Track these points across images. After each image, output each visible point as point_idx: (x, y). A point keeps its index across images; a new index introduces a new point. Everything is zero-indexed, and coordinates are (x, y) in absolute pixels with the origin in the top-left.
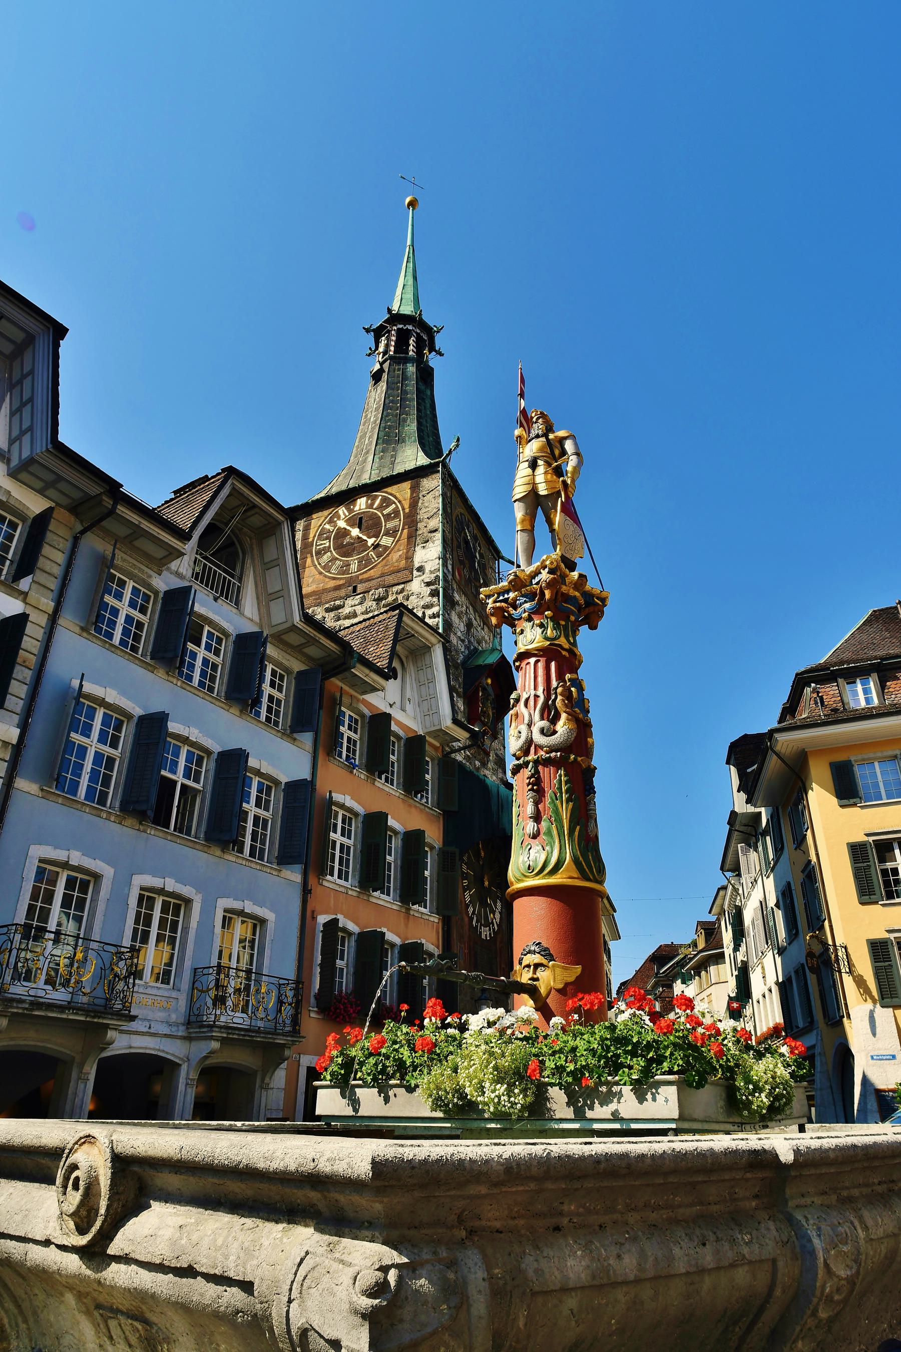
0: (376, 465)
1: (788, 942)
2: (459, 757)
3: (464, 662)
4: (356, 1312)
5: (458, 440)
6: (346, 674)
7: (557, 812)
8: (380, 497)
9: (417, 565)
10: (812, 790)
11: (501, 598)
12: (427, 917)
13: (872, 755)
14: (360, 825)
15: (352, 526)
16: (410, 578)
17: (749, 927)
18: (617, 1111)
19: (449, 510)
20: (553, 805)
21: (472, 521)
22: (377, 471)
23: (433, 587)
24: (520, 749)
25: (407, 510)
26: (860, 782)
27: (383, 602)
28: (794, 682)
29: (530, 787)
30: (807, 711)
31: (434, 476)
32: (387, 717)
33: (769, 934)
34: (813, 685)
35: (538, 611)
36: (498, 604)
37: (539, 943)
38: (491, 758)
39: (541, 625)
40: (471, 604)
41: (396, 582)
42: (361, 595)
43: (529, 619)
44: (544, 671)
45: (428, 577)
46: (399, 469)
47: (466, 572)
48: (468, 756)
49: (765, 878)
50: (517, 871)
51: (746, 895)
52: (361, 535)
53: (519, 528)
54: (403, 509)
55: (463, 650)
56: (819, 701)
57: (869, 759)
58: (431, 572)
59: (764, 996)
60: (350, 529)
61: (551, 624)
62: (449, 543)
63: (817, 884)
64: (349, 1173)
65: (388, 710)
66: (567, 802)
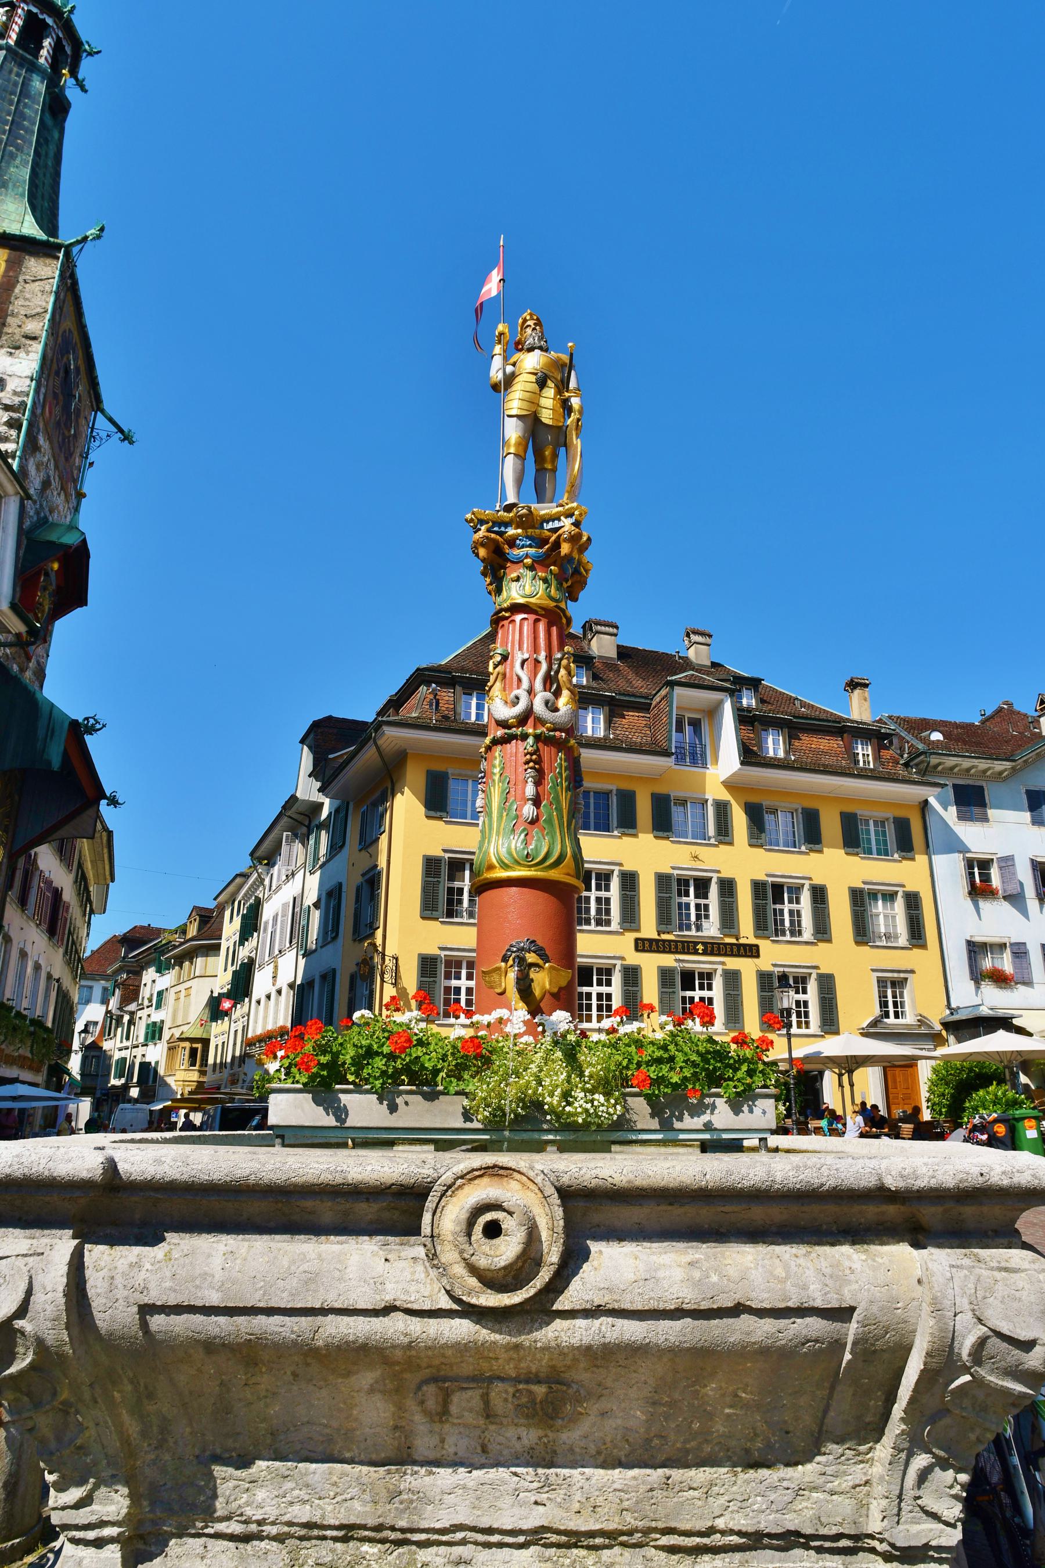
1: (320, 944)
5: (102, 230)
10: (402, 794)
11: (496, 529)
13: (469, 773)
17: (266, 923)
18: (710, 1122)
19: (58, 317)
23: (15, 415)
26: (451, 796)
28: (411, 676)
30: (419, 711)
31: (48, 261)
33: (297, 931)
36: (493, 535)
37: (533, 942)
38: (31, 665)
39: (545, 580)
40: (54, 457)
43: (531, 568)
47: (57, 410)
48: (7, 655)
49: (308, 874)
51: (274, 888)
53: (512, 450)
55: (31, 514)
57: (466, 776)
58: (15, 393)
59: (268, 997)
61: (554, 583)
62: (48, 362)
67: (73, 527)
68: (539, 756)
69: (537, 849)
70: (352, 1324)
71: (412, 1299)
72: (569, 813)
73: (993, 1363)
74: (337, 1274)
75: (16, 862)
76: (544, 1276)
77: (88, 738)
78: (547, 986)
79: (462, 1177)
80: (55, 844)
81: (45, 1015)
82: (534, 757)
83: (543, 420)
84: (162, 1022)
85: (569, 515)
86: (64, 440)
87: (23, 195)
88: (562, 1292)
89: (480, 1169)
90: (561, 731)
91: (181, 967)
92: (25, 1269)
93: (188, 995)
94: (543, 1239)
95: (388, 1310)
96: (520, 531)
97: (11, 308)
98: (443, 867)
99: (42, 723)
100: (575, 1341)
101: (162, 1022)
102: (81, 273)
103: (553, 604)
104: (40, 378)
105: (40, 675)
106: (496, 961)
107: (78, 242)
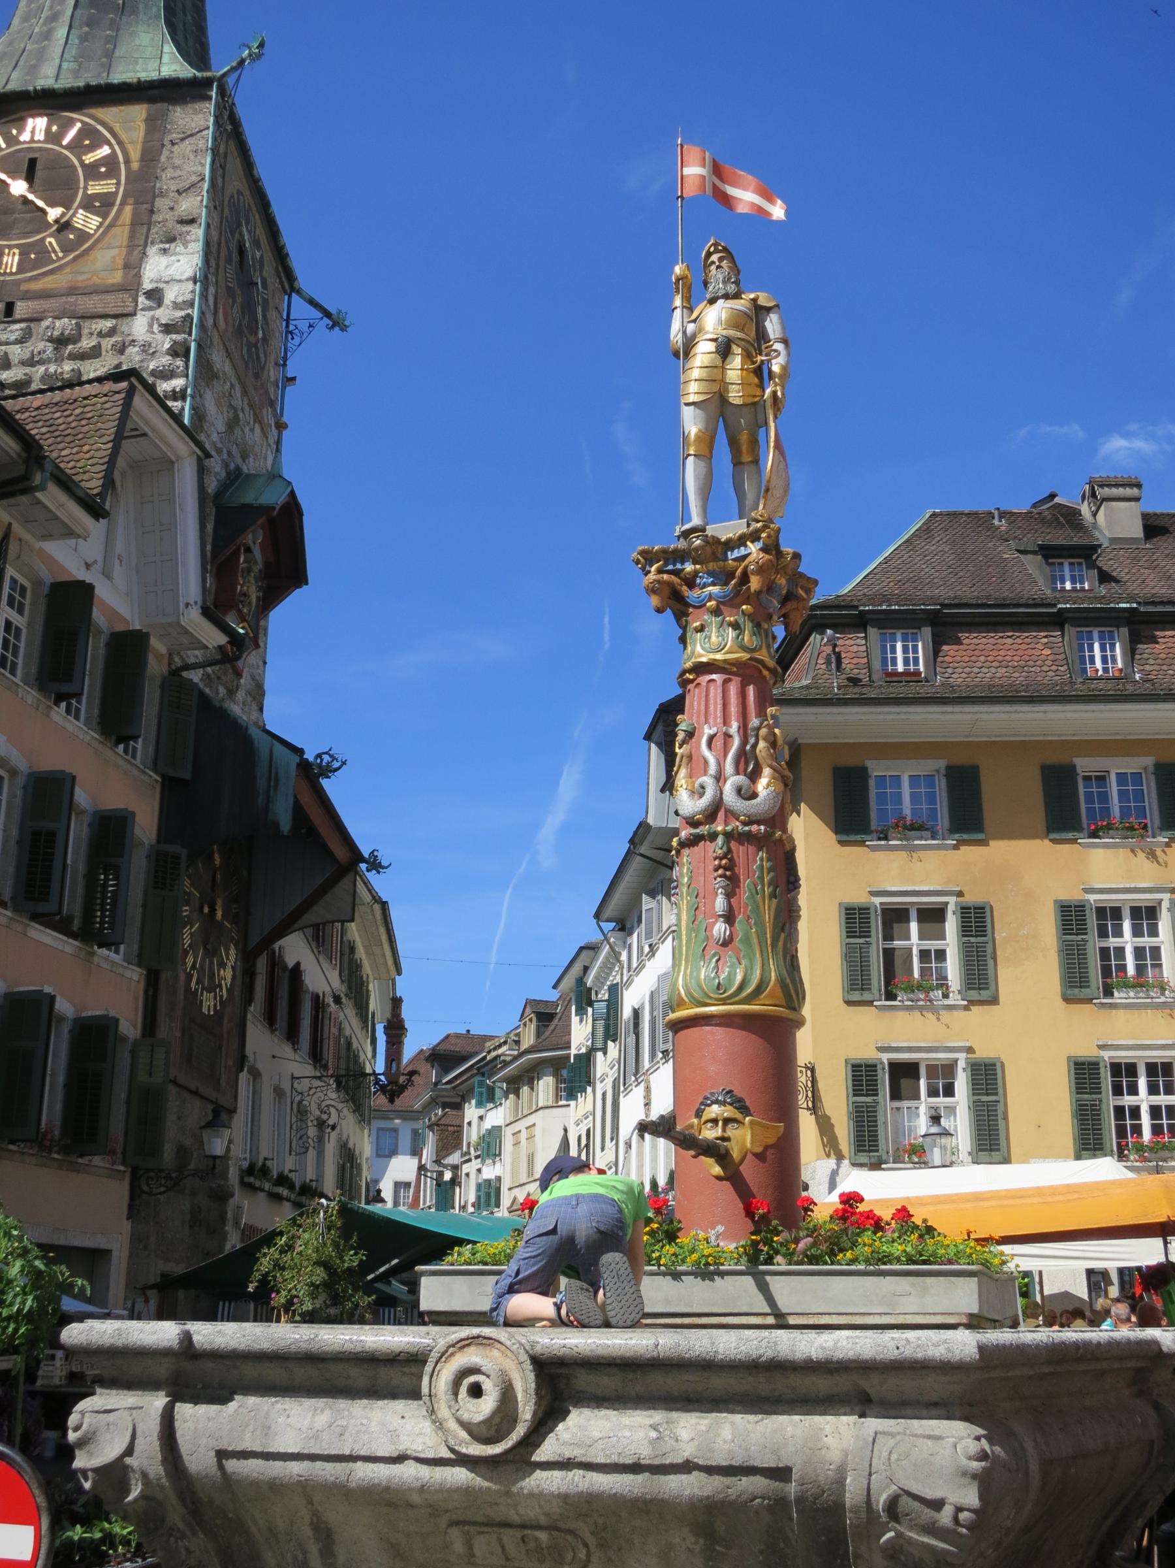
0: (72, 51)
2: (195, 676)
3: (219, 494)
4: (964, 1474)
5: (261, 45)
6: (24, 499)
7: (757, 912)
8: (79, 125)
9: (147, 285)
11: (670, 567)
12: (120, 970)
14: (19, 792)
15: (13, 175)
16: (130, 309)
19: (220, 180)
21: (254, 209)
22: (72, 65)
25: (135, 166)
27: (70, 347)
29: (720, 872)
30: (812, 674)
31: (198, 106)
32: (83, 592)
34: (829, 632)
35: (731, 602)
36: (665, 577)
37: (730, 1092)
38: (242, 681)
39: (735, 626)
41: (100, 310)
42: (23, 325)
43: (716, 612)
44: (737, 699)
45: (165, 314)
46: (120, 75)
47: (236, 311)
50: (697, 988)
51: (635, 964)
52: (31, 197)
54: (127, 161)
56: (833, 660)
58: (176, 306)
60: (9, 181)
61: (748, 627)
62: (214, 250)
64: (947, 1356)
65: (81, 575)
66: (770, 899)
67: (275, 476)
68: (731, 860)
69: (731, 978)
70: (375, 1469)
71: (420, 1449)
72: (774, 926)
73: (910, 1520)
74: (363, 1428)
75: (254, 965)
76: (520, 1431)
77: (324, 782)
78: (749, 1145)
79: (453, 1346)
80: (309, 931)
81: (320, 1177)
82: (724, 862)
83: (731, 400)
84: (499, 1179)
85: (754, 537)
86: (249, 350)
87: (157, 17)
88: (539, 1446)
89: (467, 1339)
90: (758, 823)
91: (518, 1096)
92: (130, 1419)
93: (531, 1138)
94: (519, 1400)
95: (400, 1459)
96: (698, 567)
97: (158, 186)
98: (873, 920)
99: (261, 770)
100: (554, 1489)
101: (499, 1179)
102: (243, 112)
104: (206, 277)
105: (258, 694)
106: (689, 1118)
107: (233, 69)
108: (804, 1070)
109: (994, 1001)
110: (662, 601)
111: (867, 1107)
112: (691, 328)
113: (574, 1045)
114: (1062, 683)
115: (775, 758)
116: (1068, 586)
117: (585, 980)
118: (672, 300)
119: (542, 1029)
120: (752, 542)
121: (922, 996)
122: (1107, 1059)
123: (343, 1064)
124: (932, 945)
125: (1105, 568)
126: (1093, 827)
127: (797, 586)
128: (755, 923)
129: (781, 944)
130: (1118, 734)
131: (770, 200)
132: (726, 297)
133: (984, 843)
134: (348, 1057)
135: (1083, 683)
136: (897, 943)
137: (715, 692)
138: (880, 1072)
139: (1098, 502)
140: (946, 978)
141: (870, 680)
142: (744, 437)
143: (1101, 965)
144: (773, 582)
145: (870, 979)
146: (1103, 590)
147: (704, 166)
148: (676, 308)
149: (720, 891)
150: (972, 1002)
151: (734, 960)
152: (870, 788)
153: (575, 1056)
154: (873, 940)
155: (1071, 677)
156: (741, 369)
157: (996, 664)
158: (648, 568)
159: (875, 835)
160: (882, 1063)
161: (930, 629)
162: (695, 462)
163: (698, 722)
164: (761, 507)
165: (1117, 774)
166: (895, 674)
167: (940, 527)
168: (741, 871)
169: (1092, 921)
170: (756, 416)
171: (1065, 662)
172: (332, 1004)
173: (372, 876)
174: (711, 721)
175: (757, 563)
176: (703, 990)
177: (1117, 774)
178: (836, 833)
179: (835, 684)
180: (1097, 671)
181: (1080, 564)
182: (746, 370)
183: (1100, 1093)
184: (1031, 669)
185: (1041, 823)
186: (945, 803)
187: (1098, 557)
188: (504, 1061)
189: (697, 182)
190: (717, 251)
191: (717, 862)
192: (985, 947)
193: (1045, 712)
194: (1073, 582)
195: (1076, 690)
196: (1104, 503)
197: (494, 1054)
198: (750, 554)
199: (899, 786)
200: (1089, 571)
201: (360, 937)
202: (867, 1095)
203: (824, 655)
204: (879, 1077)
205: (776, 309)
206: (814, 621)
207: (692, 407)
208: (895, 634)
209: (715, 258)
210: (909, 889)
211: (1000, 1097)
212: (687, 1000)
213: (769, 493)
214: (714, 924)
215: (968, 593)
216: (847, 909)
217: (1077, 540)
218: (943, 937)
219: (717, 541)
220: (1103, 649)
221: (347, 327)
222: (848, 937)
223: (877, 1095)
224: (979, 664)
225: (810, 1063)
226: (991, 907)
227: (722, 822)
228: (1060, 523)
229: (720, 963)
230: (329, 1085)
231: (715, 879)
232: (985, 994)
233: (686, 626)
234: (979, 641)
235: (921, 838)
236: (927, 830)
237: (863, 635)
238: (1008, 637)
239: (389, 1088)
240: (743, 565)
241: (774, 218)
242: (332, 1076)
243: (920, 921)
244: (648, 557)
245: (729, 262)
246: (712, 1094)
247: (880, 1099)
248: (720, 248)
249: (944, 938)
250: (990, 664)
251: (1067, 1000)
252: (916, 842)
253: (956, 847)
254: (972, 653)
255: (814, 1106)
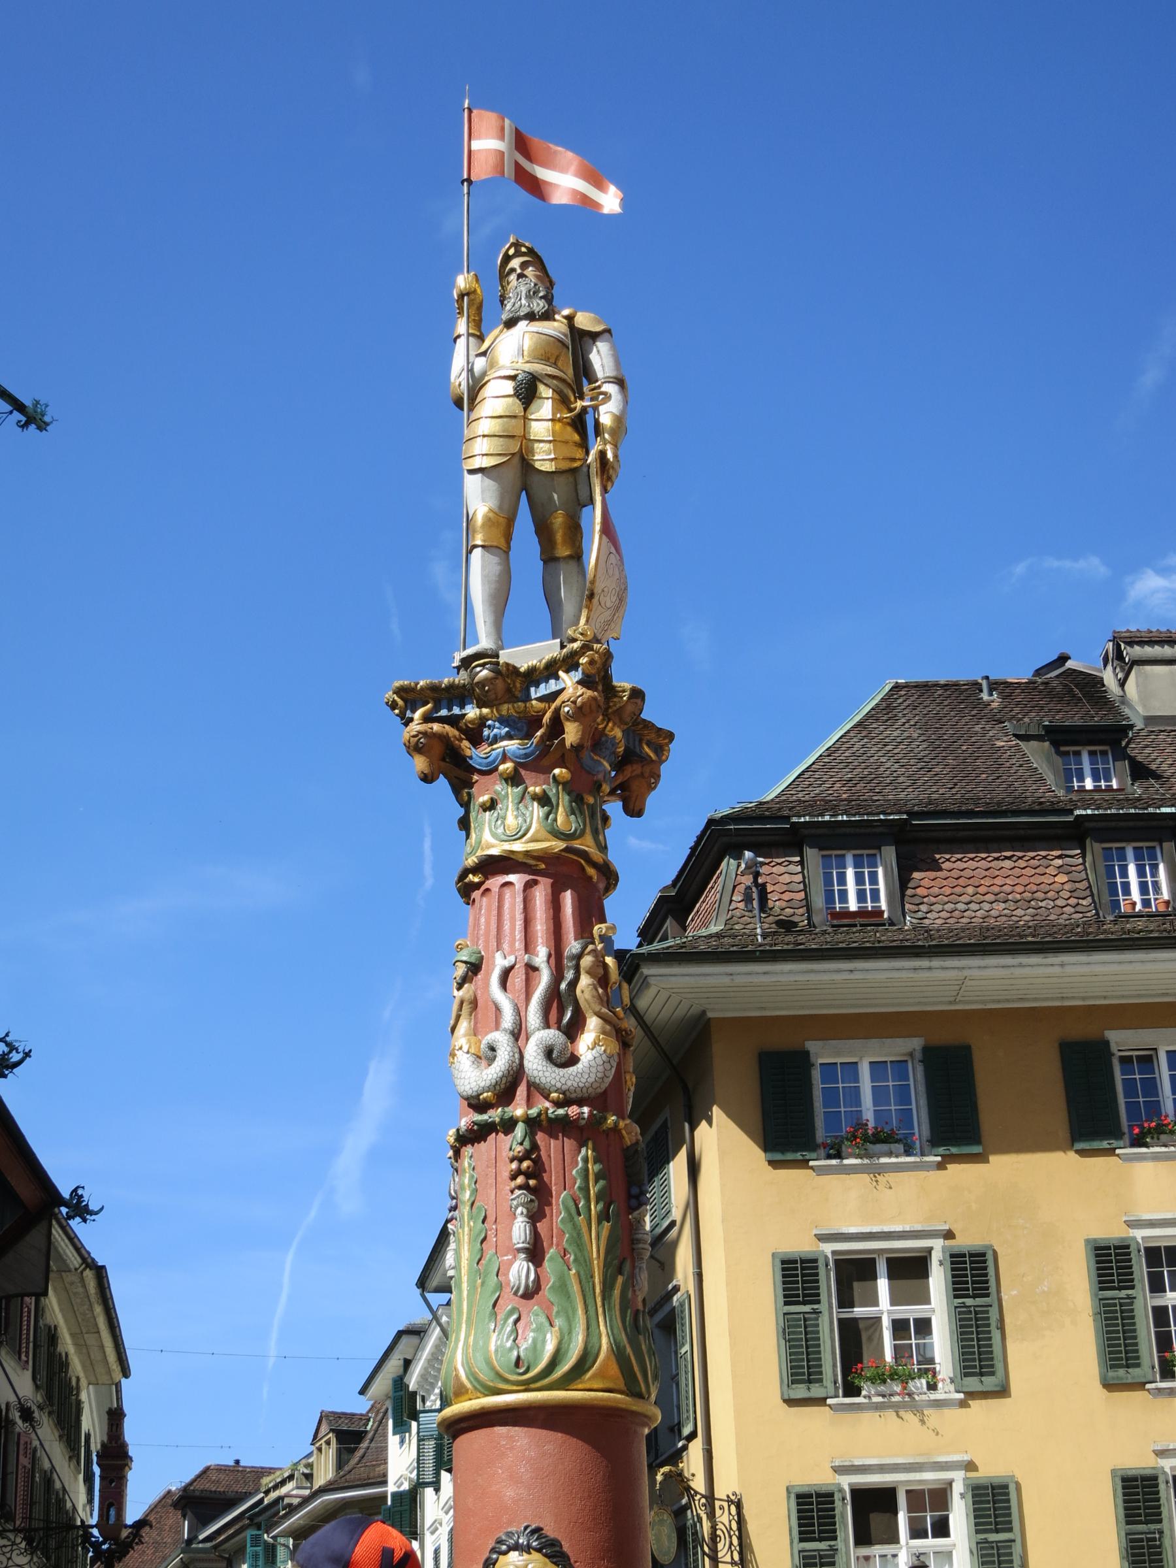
7: (578, 1241)
11: (444, 712)
20: (570, 1226)
24: (493, 1087)
29: (520, 1180)
30: (723, 918)
34: (748, 854)
35: (537, 763)
36: (436, 727)
37: (538, 1530)
39: (543, 800)
43: (514, 779)
56: (755, 896)
61: (564, 799)
63: (687, 1347)
66: (599, 1222)
68: (538, 1162)
69: (536, 1348)
72: (607, 1265)
82: (525, 1164)
83: (538, 465)
85: (569, 662)
90: (580, 1103)
96: (485, 711)
103: (562, 845)
108: (725, 1504)
109: (1003, 1391)
110: (431, 763)
111: (821, 1557)
112: (480, 364)
113: (392, 1479)
114: (1084, 923)
115: (606, 1001)
116: (1089, 784)
117: (405, 1380)
118: (453, 325)
119: (345, 1456)
120: (567, 671)
121: (897, 1388)
122: (1168, 1470)
123: (38, 1512)
124: (911, 1312)
125: (1139, 758)
126: (1137, 1131)
127: (641, 741)
128: (575, 1260)
129: (617, 1292)
130: (1167, 994)
131: (599, 185)
132: (531, 317)
133: (981, 1158)
134: (48, 1502)
135: (1115, 922)
136: (859, 1311)
137: (513, 902)
138: (838, 1504)
139: (1127, 667)
140: (932, 1361)
141: (809, 924)
142: (558, 520)
143: (1156, 1333)
144: (603, 733)
145: (821, 1366)
146: (1138, 790)
147: (502, 138)
148: (459, 336)
149: (520, 1210)
150: (971, 1395)
151: (543, 1319)
152: (814, 1082)
153: (394, 1495)
154: (823, 1307)
155: (1097, 914)
156: (552, 420)
157: (990, 897)
158: (409, 714)
159: (822, 1152)
160: (841, 1490)
161: (893, 848)
162: (483, 556)
163: (486, 947)
164: (583, 621)
165: (1168, 1052)
166: (846, 914)
167: (906, 704)
168: (553, 1178)
169: (1141, 1269)
170: (576, 490)
171: (1088, 892)
172: (19, 1422)
173: (75, 1223)
174: (506, 946)
175: (574, 702)
176: (493, 1368)
177: (1168, 1052)
178: (766, 1148)
179: (759, 931)
180: (1134, 904)
181: (1104, 753)
182: (560, 420)
183: (1160, 1521)
184: (1041, 904)
185: (1063, 1132)
186: (923, 1102)
187: (1128, 743)
188: (290, 1505)
189: (492, 161)
190: (518, 254)
191: (514, 1166)
192: (987, 1312)
193: (1062, 965)
194: (1096, 778)
195: (1105, 932)
196: (1135, 668)
197: (273, 1495)
198: (563, 690)
199: (856, 1079)
200: (1118, 764)
201: (66, 1321)
202: (821, 1540)
203: (741, 888)
204: (837, 1512)
205: (607, 335)
206: (725, 839)
207: (479, 476)
208: (844, 856)
209: (515, 263)
210: (875, 1229)
211: (1015, 1534)
212: (469, 1385)
213: (595, 601)
214: (511, 1263)
215: (941, 792)
216: (783, 1262)
217: (1098, 719)
218: (926, 1300)
219: (513, 671)
220: (1141, 873)
221: (47, 424)
222: (786, 1303)
223: (835, 1539)
224: (965, 898)
225: (734, 1494)
226: (995, 1253)
227: (524, 1102)
228: (1074, 696)
229: (520, 1325)
230: (14, 1544)
231: (512, 1192)
232: (989, 1382)
233: (469, 802)
234: (965, 865)
235: (890, 1154)
236: (897, 1141)
237: (798, 859)
238: (1007, 858)
239: (105, 1547)
240: (553, 706)
241: (606, 211)
242: (20, 1531)
243: (891, 1277)
244: (409, 698)
245: (537, 269)
246: (510, 1534)
247: (839, 1544)
248: (523, 249)
249: (928, 1302)
250: (982, 898)
251: (1109, 1386)
252: (884, 1160)
253: (941, 1166)
254: (955, 882)
255: (741, 1559)
